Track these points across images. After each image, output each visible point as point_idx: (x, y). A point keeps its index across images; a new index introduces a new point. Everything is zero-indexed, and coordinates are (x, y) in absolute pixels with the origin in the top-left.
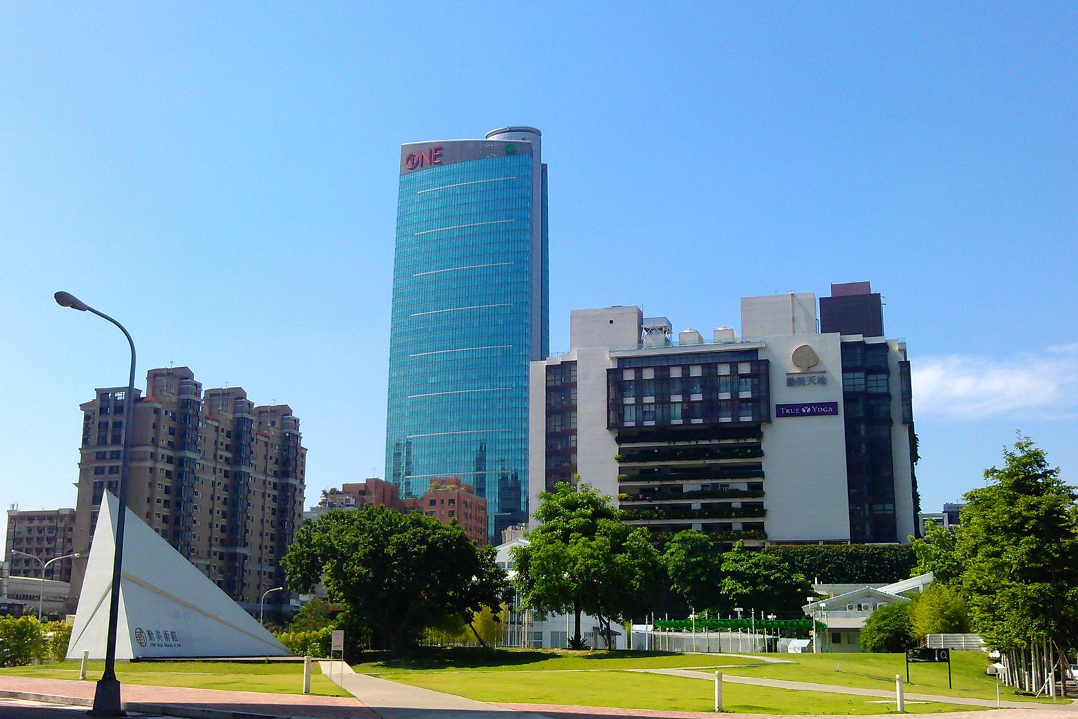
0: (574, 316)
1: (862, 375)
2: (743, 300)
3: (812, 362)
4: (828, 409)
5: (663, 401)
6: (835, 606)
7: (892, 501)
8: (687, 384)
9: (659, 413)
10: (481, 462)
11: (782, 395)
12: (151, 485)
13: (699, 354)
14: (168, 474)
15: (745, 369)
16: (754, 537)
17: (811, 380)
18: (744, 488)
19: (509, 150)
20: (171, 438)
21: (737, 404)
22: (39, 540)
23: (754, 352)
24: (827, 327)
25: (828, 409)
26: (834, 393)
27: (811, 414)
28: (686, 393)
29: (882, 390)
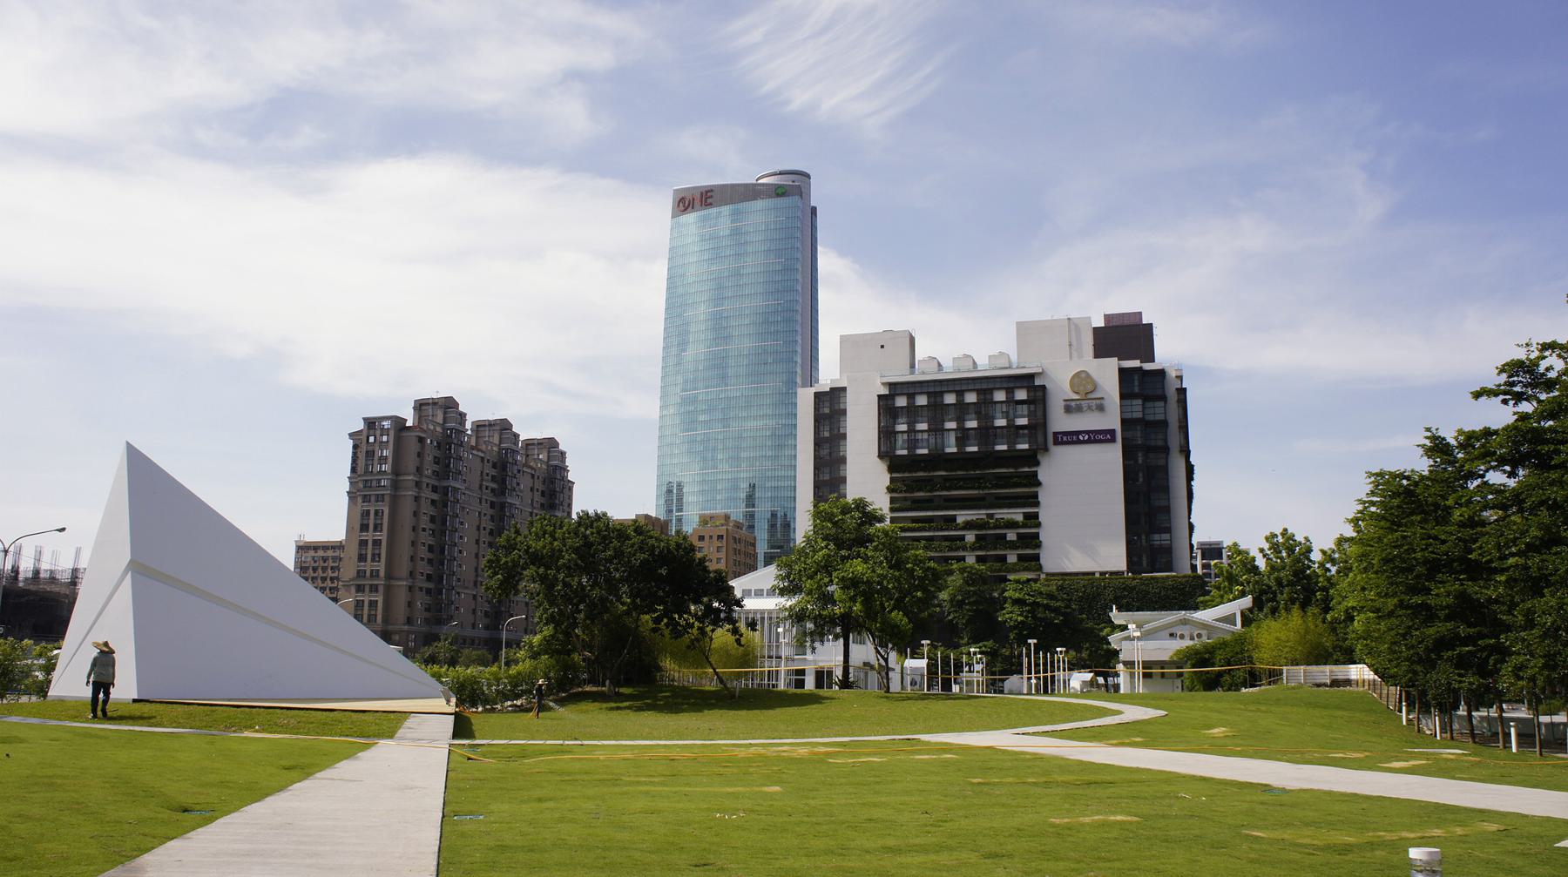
0: (844, 340)
1: (1140, 402)
2: (1018, 323)
3: (1090, 387)
4: (1105, 437)
5: (937, 429)
6: (1140, 638)
7: (1168, 530)
8: (961, 410)
9: (932, 441)
10: (750, 500)
11: (1060, 422)
12: (415, 514)
13: (973, 379)
14: (433, 502)
15: (1021, 395)
16: (1027, 569)
17: (1090, 408)
18: (1020, 518)
19: (779, 192)
20: (436, 468)
21: (1013, 431)
22: (324, 569)
23: (1031, 377)
24: (1099, 353)
25: (1105, 437)
26: (1111, 420)
27: (1089, 441)
28: (960, 420)
29: (1160, 417)
